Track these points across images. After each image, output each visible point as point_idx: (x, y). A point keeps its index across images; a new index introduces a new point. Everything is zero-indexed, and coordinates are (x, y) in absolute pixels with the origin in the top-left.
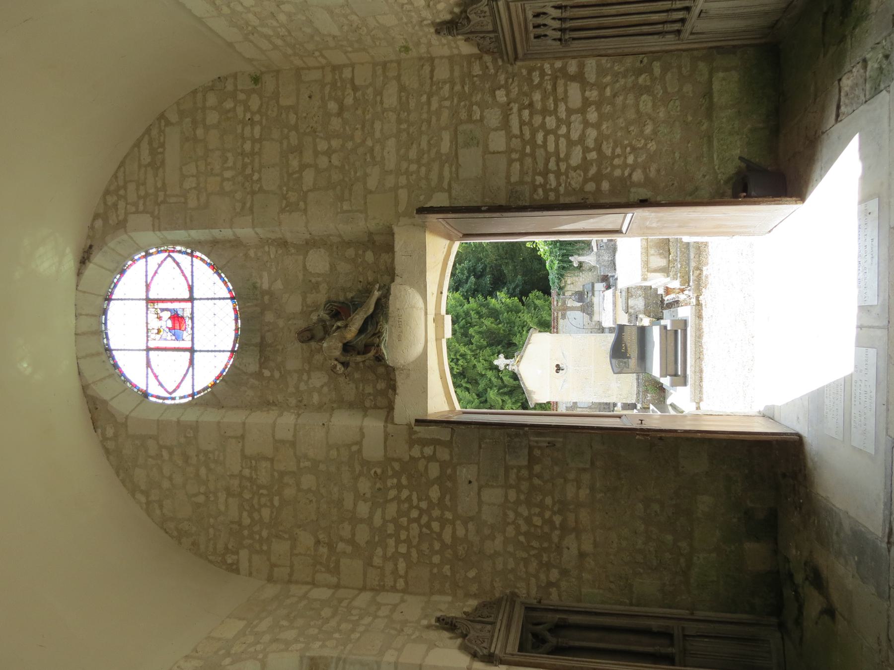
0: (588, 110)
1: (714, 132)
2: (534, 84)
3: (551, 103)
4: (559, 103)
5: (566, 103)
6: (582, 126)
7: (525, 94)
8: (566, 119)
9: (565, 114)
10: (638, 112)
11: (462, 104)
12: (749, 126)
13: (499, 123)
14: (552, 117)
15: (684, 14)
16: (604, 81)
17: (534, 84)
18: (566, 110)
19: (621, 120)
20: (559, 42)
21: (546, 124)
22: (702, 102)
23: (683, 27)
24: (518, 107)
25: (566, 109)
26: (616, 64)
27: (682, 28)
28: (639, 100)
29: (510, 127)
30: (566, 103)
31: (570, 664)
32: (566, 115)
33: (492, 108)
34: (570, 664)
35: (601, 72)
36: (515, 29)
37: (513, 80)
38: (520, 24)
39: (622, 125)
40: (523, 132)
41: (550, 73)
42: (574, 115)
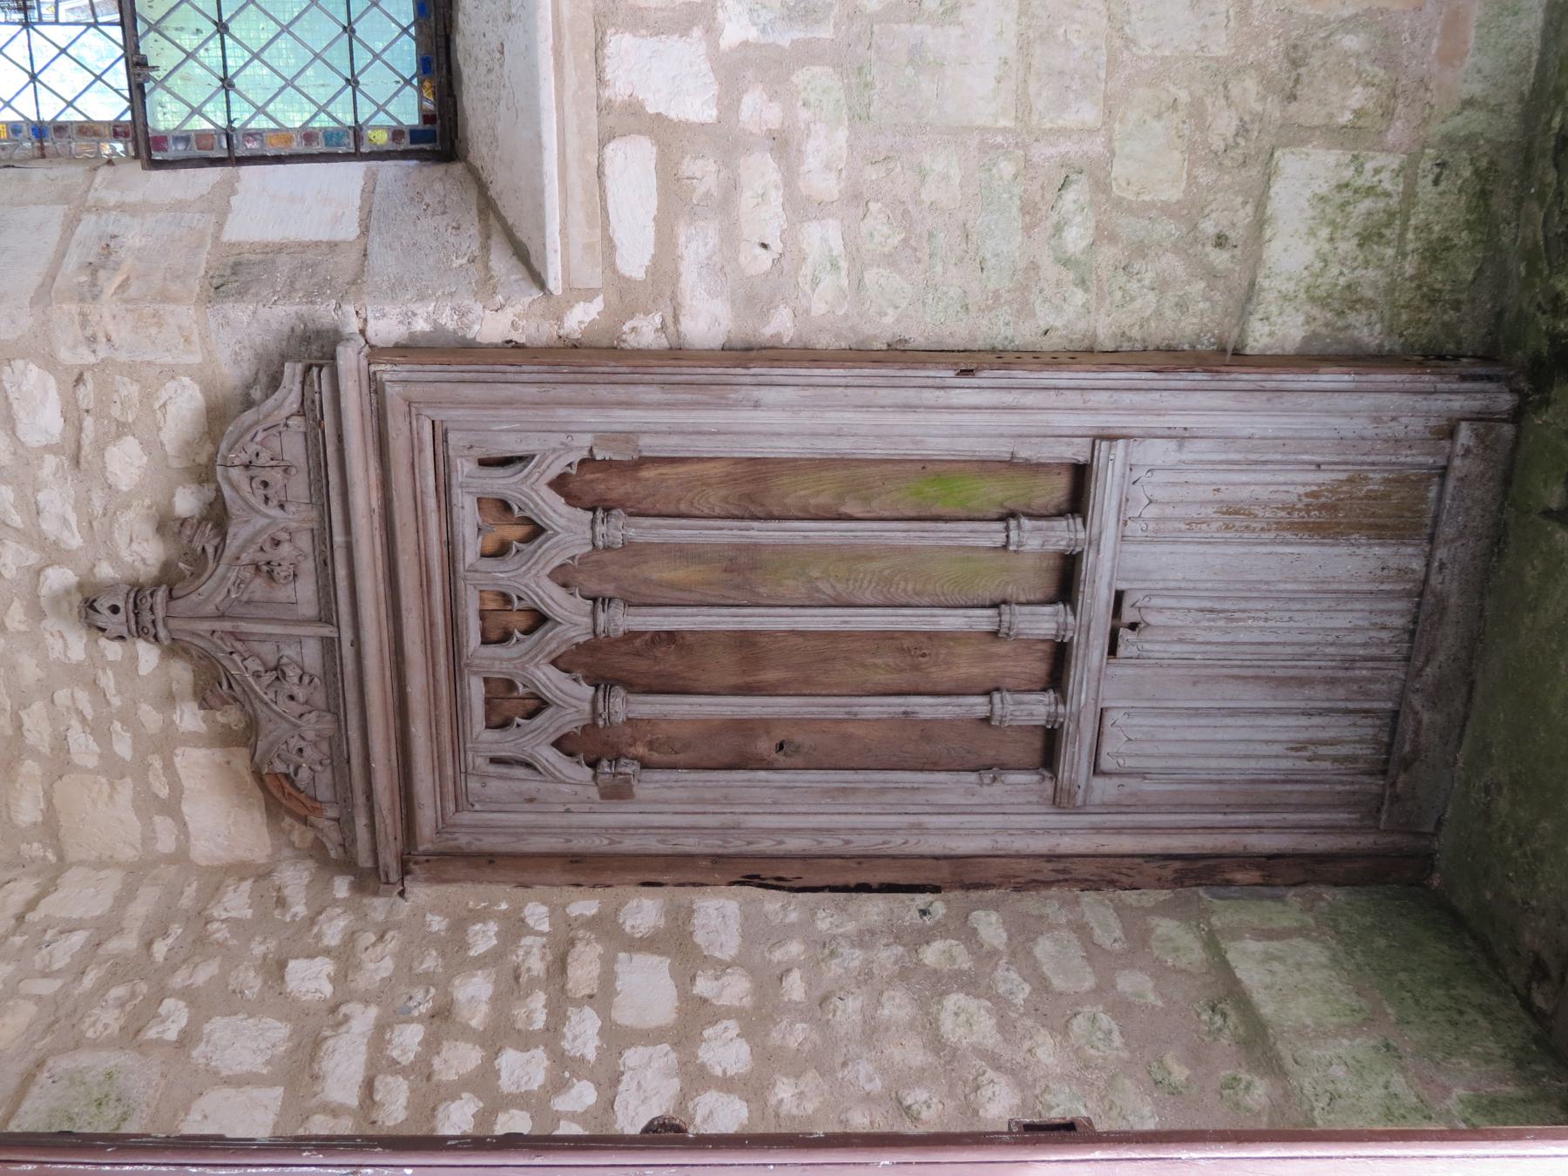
0: (706, 1033)
1: (1312, 1109)
2: (472, 953)
3: (536, 1009)
4: (572, 1012)
5: (604, 1012)
6: (675, 1084)
7: (427, 979)
8: (599, 1059)
9: (596, 1042)
10: (936, 1043)
11: (118, 992)
12: (1459, 1091)
13: (268, 1063)
14: (533, 1052)
15: (1056, 614)
16: (778, 955)
17: (472, 953)
18: (602, 1032)
19: (864, 1068)
20: (589, 771)
21: (499, 1078)
22: (1212, 1022)
23: (1065, 704)
24: (378, 1019)
25: (601, 1028)
26: (821, 914)
27: (1061, 709)
28: (934, 1009)
29: (315, 1078)
30: (604, 1012)
31: (932, 373)
32: (598, 1048)
33: (250, 1016)
34: (932, 373)
35: (756, 933)
36: (404, 604)
37: (381, 938)
38: (429, 626)
39: (868, 1087)
40: (377, 1098)
41: (545, 927)
42: (641, 1049)
